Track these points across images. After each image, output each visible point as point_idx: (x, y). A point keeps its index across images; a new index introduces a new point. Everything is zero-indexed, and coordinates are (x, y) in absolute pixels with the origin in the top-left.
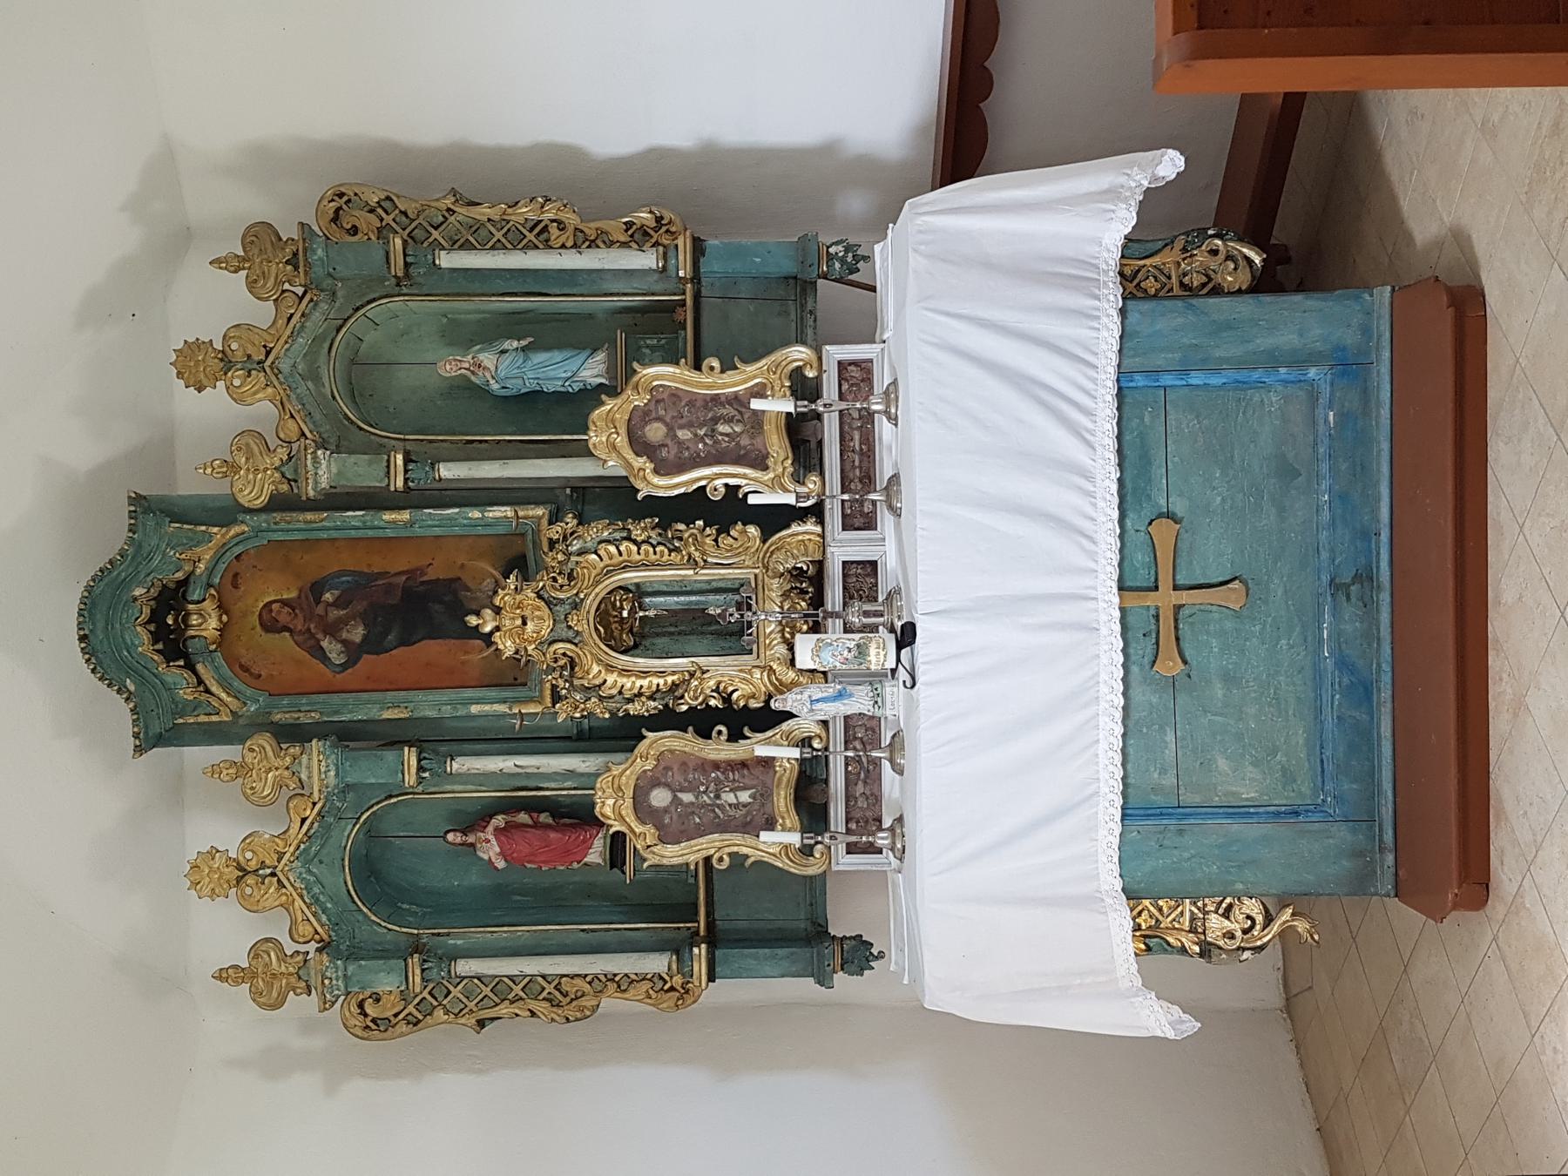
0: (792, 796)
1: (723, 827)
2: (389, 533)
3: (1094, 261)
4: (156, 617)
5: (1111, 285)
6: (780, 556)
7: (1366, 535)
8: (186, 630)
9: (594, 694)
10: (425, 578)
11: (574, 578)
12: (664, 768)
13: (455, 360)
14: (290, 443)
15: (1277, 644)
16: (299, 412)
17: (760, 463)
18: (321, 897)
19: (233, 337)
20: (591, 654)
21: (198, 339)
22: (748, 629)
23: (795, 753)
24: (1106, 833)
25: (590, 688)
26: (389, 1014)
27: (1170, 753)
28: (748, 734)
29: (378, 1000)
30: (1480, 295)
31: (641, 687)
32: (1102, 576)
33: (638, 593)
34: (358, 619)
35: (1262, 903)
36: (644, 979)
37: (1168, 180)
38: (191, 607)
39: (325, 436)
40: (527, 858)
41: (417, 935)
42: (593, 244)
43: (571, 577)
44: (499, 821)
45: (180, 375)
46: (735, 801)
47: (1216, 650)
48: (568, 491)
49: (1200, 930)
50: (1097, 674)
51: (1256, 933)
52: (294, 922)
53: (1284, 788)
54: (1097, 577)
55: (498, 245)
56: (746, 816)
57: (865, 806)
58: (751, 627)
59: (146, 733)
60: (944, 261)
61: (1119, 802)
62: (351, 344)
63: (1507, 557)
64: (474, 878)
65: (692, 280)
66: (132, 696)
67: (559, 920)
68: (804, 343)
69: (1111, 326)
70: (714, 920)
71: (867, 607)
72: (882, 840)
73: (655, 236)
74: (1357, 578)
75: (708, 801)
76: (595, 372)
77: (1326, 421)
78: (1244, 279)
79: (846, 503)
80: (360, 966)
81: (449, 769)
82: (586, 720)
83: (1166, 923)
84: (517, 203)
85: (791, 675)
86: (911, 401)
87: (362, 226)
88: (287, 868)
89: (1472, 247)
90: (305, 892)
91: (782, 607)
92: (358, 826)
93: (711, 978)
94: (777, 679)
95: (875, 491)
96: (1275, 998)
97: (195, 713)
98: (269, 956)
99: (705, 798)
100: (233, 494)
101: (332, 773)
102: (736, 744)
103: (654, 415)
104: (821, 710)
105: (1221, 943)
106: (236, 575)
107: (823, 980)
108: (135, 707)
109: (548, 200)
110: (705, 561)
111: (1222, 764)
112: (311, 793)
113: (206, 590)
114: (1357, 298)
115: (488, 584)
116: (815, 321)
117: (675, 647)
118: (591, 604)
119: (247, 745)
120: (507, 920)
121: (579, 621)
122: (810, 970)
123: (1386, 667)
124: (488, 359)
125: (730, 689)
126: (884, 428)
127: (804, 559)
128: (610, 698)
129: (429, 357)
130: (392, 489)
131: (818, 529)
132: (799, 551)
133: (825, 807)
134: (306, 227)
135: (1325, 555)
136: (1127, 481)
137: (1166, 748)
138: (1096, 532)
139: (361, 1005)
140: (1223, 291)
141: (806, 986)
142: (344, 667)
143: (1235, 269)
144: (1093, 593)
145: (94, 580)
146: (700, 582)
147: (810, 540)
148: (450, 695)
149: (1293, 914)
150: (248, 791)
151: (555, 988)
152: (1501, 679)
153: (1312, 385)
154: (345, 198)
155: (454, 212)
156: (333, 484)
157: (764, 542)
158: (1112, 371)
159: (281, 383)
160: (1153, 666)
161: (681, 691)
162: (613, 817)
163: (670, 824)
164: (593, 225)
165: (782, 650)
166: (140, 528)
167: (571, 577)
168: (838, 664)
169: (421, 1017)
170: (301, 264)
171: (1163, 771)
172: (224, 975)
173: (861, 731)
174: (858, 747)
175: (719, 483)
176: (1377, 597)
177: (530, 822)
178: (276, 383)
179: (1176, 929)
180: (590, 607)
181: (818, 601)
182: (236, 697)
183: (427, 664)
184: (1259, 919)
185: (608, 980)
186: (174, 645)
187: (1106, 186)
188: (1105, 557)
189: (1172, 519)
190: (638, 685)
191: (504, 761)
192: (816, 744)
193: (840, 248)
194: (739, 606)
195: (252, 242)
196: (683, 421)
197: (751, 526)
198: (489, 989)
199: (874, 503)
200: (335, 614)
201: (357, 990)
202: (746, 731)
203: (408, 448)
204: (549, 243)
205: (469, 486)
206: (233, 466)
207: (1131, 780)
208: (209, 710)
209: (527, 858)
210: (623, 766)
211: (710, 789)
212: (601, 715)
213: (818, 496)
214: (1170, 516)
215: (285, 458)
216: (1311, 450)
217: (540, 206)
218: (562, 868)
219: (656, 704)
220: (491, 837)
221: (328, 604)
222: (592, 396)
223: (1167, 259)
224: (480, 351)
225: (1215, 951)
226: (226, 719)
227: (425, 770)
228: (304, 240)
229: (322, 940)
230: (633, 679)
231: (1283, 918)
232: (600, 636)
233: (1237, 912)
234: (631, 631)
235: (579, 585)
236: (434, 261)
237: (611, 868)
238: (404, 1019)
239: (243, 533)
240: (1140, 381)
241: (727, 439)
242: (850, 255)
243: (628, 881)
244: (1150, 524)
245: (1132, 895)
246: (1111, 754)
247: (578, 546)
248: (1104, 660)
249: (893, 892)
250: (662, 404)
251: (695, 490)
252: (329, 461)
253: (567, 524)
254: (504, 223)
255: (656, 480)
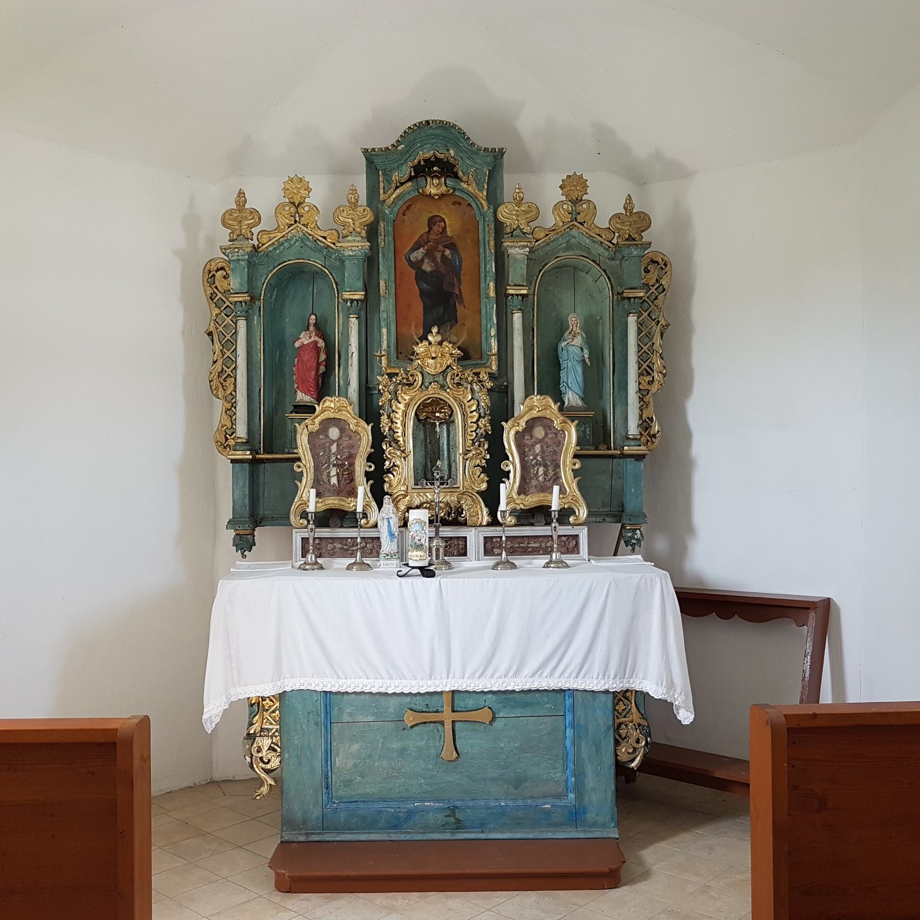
0: (334, 507)
1: (317, 469)
2: (483, 285)
3: (634, 676)
4: (438, 162)
5: (621, 685)
6: (469, 501)
7: (482, 826)
8: (430, 177)
9: (393, 396)
10: (457, 304)
11: (458, 386)
12: (350, 435)
13: (577, 323)
14: (532, 234)
15: (421, 777)
16: (549, 239)
17: (522, 490)
18: (282, 247)
19: (589, 205)
20: (416, 395)
21: (588, 187)
22: (430, 483)
23: (359, 509)
24: (317, 682)
25: (396, 393)
26: (217, 284)
27: (360, 718)
28: (369, 483)
29: (225, 278)
30: (616, 886)
31: (397, 423)
32: (460, 682)
33: (449, 422)
34: (435, 268)
35: (277, 768)
36: (232, 424)
37: (677, 715)
38: (443, 179)
39: (536, 252)
40: (300, 359)
41: (260, 299)
42: (641, 400)
43: (458, 384)
44: (321, 344)
45: (569, 177)
46: (331, 475)
47: (419, 744)
48: (505, 384)
49: (262, 734)
50: (405, 679)
51: (260, 764)
52: (269, 232)
53: (341, 781)
54: (460, 679)
55: (640, 348)
56: (323, 481)
57: (328, 548)
58: (431, 485)
59: (375, 155)
60: (636, 593)
61: (334, 690)
62: (585, 268)
63: (473, 902)
64: (289, 331)
65: (622, 454)
66: (395, 148)
67: (266, 376)
68: (588, 516)
69: (599, 686)
70: (264, 463)
71: (441, 550)
72: (310, 557)
73: (645, 434)
74: (458, 821)
75: (331, 460)
76: (571, 399)
77: (545, 803)
78: (623, 757)
79: (499, 539)
80: (244, 268)
81: (351, 316)
82: (377, 392)
83: (266, 715)
84: (662, 359)
85: (403, 507)
86: (555, 574)
87: (649, 276)
88: (299, 229)
89: (640, 881)
90: (286, 238)
91: (441, 502)
92: (321, 267)
93: (233, 461)
94: (400, 499)
95: (507, 555)
96: (218, 775)
97: (385, 181)
98: (251, 219)
99: (334, 458)
100: (504, 203)
101: (351, 253)
102: (364, 476)
103: (548, 431)
104: (383, 524)
105: (255, 745)
106: (460, 204)
107: (231, 524)
108: (389, 150)
109: (664, 375)
110: (467, 459)
111: (355, 747)
112: (340, 242)
113: (452, 188)
114: (612, 819)
115: (454, 339)
116: (599, 522)
117: (419, 443)
118: (443, 395)
119: (367, 208)
120: (267, 348)
121: (434, 388)
122: (236, 516)
123: (408, 837)
124: (578, 341)
125: (395, 473)
126: (542, 560)
127: (468, 515)
128: (390, 405)
129: (578, 309)
130: (508, 287)
131: (484, 523)
132: (473, 512)
133: (327, 526)
134: (648, 246)
135: (471, 803)
136: (513, 695)
137: (364, 716)
138: (485, 678)
139: (222, 268)
140: (617, 746)
141: (227, 514)
142: (409, 260)
143: (629, 753)
144: (451, 675)
145: (459, 129)
146: (455, 457)
147: (479, 518)
148: (393, 317)
149: (271, 785)
150: (342, 209)
151: (229, 375)
152: (405, 899)
153: (565, 796)
154: (664, 267)
155: (657, 325)
156: (510, 255)
157: (477, 493)
158: (575, 686)
159: (565, 230)
160: (410, 709)
161: (394, 445)
162: (323, 407)
163: (318, 438)
164: (651, 400)
165: (417, 502)
166: (487, 154)
167: (458, 384)
168: (411, 534)
169: (214, 301)
170: (630, 243)
171: (351, 714)
172: (241, 195)
173: (372, 547)
174: (362, 545)
175: (511, 468)
176: (448, 832)
177: (320, 361)
178: (565, 227)
179: (263, 721)
180: (442, 395)
181: (445, 523)
182: (393, 203)
183: (409, 306)
184: (268, 767)
185: (232, 404)
186: (422, 171)
187: (675, 682)
188: (471, 683)
189: (492, 720)
190: (398, 421)
191: (355, 346)
192: (363, 521)
193: (639, 536)
194: (442, 478)
195: (640, 217)
196: (545, 448)
197: (486, 486)
198: (229, 338)
199: (501, 554)
200: (438, 256)
201: (231, 266)
202: (371, 482)
203: (530, 296)
204: (641, 376)
205: (509, 329)
206: (520, 203)
207: (345, 697)
208: (386, 188)
209: (300, 359)
210: (352, 412)
211: (339, 461)
212: (380, 400)
213: (505, 523)
214: (494, 719)
215: (524, 231)
216: (530, 795)
217: (661, 371)
218: (294, 378)
219: (387, 431)
220: (312, 339)
221: (443, 252)
222: (558, 397)
223: (635, 716)
224: (582, 336)
225: (250, 742)
226: (381, 198)
227: (351, 303)
228: (642, 244)
229: (259, 248)
230: (401, 419)
231: (268, 780)
232: (425, 400)
233: (272, 754)
234: (428, 418)
235: (454, 389)
236: (631, 313)
237: (293, 406)
238: (214, 291)
239: (483, 208)
240: (569, 702)
241: (535, 472)
242: (635, 542)
243: (286, 415)
244: (489, 708)
245: (282, 696)
246: (361, 686)
247: (476, 389)
248: (413, 683)
249: (280, 564)
250: (555, 436)
251: (506, 454)
252: (523, 254)
253: (488, 383)
254: (652, 351)
255: (512, 432)
